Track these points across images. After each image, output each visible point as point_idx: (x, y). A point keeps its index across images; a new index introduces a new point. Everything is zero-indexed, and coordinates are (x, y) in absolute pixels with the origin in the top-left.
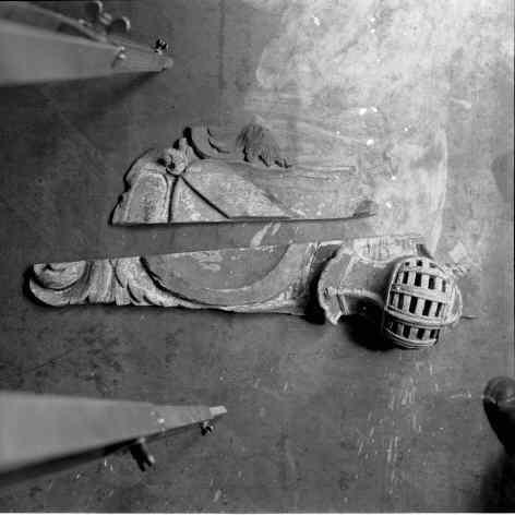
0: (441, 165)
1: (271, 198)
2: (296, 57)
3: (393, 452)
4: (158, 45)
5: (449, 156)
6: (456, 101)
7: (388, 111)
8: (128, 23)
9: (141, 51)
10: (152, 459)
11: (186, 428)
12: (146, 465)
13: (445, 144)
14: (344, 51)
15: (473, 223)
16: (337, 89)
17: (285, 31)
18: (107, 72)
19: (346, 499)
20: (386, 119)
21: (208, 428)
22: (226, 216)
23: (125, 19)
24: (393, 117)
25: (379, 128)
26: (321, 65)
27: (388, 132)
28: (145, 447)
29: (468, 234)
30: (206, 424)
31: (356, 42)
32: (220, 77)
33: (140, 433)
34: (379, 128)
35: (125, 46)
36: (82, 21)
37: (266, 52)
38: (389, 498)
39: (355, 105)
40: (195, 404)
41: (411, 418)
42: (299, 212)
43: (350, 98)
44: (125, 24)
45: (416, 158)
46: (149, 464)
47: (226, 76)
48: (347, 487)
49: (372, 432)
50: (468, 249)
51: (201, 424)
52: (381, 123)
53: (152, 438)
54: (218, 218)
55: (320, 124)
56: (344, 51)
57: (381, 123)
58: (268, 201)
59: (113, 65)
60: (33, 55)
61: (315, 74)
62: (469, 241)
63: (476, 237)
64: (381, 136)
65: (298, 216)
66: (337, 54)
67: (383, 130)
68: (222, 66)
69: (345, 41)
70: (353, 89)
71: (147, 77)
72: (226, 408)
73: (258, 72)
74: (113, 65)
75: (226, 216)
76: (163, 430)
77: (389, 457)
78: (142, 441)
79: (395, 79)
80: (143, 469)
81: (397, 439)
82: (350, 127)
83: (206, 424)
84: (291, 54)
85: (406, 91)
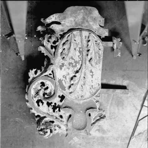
0: (101, 134)
1: (140, 134)
2: (132, 92)
3: (18, 120)
4: (140, 54)
5: (104, 137)
6: (120, 139)
7: (117, 119)
8: (145, 45)
9: (138, 48)
10: (9, 38)
11: (18, 49)
12: (7, 36)
13: (107, 136)
14: (134, 106)
15: (84, 144)
16: (123, 104)
17: (140, 89)
18: (132, 39)
19: (5, 106)
20: (114, 118)
21: (18, 55)
22: (139, 120)
23: (146, 44)
24: (115, 120)
25: (112, 116)
26: (130, 99)
27: (111, 119)
28: (12, 36)
29: (81, 142)
30: (19, 54)
31: (137, 110)
32: (126, 70)
33: (16, 35)
34: (112, 116)
35: (139, 44)
36: (146, 32)
37: (134, 83)
38: (5, 119)
39: (118, 109)
40: (25, 52)
41: (28, 125)
42: (133, 139)
43: (120, 108)
44: (145, 44)
45: (103, 127)
46: (7, 38)
47: (127, 72)
48: (9, 106)
49: (25, 114)
50: (76, 142)
51: (19, 53)
52: (113, 117)
53: (15, 38)
54: (140, 118)
55: (113, 98)
56: (134, 106)
57: (113, 117)
58: (139, 133)
59: (133, 40)
60: (134, 13)
61: (127, 98)
62: (79, 143)
63: (80, 144)
64: (110, 117)
65: (132, 139)
66: (133, 104)
67: (111, 117)
68: (129, 70)
69: (137, 107)
70: (123, 108)
71: (131, 52)
72: (24, 61)
73: (127, 81)
74: (133, 40)
75: (139, 120)
76: (17, 42)
77: (17, 119)
78: (14, 36)
79: (126, 121)
80: (6, 36)
81: (22, 121)
82: (112, 108)
83: (19, 54)
84: (133, 91)
85: (123, 124)
